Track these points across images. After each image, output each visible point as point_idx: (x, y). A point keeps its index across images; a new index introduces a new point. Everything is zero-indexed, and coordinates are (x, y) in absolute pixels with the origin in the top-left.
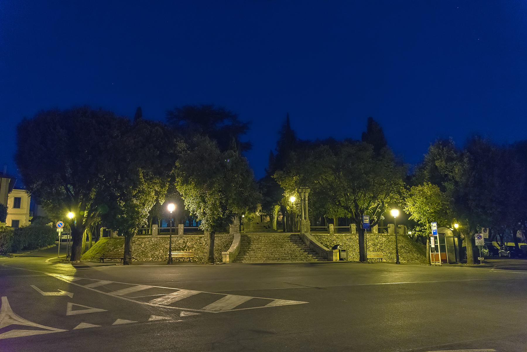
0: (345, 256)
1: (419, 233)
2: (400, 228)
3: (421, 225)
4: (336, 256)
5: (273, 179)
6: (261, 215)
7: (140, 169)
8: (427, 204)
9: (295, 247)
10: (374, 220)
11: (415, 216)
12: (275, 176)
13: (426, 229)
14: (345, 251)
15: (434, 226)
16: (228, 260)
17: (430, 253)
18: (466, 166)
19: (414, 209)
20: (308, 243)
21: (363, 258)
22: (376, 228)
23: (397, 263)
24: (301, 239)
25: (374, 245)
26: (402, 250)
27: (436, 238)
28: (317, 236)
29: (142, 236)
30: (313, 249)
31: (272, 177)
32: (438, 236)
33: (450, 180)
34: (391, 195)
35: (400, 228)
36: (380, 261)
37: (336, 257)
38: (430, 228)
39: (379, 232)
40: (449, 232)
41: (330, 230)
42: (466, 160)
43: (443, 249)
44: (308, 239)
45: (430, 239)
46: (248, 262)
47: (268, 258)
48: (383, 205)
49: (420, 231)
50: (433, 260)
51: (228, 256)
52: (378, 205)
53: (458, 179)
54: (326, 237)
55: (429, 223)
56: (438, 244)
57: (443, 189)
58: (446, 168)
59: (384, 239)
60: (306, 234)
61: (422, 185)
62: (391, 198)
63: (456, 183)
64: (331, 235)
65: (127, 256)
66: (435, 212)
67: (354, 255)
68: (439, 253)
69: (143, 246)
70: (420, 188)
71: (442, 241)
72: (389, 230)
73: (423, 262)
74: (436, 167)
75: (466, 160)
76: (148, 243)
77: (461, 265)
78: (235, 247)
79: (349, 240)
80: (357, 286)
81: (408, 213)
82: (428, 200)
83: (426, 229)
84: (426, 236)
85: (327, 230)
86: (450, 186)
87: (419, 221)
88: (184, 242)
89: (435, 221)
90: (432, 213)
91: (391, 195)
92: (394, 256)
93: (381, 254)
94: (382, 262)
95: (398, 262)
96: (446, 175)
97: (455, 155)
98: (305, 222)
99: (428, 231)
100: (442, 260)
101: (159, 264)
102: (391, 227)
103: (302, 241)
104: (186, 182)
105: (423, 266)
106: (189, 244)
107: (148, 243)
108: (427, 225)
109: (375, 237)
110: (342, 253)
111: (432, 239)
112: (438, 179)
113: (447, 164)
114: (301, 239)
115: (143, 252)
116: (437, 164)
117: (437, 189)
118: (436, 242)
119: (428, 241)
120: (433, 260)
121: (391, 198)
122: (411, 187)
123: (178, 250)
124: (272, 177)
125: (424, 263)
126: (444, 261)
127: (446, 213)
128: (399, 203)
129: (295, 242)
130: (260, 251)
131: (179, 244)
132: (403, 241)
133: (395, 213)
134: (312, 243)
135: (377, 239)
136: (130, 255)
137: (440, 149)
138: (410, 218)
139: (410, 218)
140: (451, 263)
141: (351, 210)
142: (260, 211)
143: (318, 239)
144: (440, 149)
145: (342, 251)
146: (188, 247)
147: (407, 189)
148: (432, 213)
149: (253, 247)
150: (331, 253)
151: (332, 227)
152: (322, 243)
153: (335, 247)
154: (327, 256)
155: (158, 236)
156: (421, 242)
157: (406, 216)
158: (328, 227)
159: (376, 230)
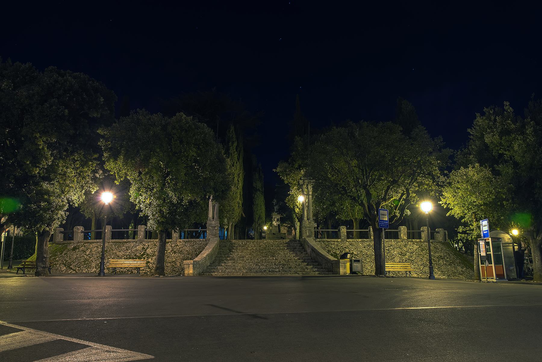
0: (359, 269)
1: (463, 235)
2: (438, 232)
3: (465, 225)
4: (345, 267)
5: (276, 173)
6: (279, 225)
7: (38, 135)
8: (472, 193)
9: (291, 256)
10: (396, 216)
11: (456, 211)
12: (278, 169)
13: (473, 230)
14: (359, 261)
15: (485, 225)
16: (191, 271)
17: (480, 265)
18: (531, 139)
19: (454, 202)
20: (309, 251)
21: (380, 269)
22: (403, 230)
23: (430, 278)
24: (301, 245)
25: (401, 254)
26: (441, 261)
27: (487, 244)
28: (324, 242)
29: (90, 241)
30: (316, 259)
31: (274, 170)
32: (490, 240)
33: (506, 161)
34: (420, 179)
35: (438, 232)
36: (407, 275)
37: (345, 269)
38: (479, 227)
39: (409, 237)
40: (506, 237)
41: (342, 234)
42: (529, 130)
43: (498, 260)
44: (309, 246)
45: (478, 245)
46: (220, 274)
47: (250, 270)
48: (408, 194)
49: (464, 232)
50: (484, 275)
51: (191, 266)
52: (403, 194)
53: (518, 159)
54: (336, 243)
55: (477, 220)
56: (492, 253)
57: (496, 173)
58: (501, 144)
59: (416, 247)
60: (307, 239)
61: (466, 167)
62: (421, 184)
63: (516, 165)
64: (342, 241)
65: (40, 264)
66: (485, 204)
67: (369, 268)
68: (493, 265)
69: (87, 253)
70: (462, 170)
71: (497, 248)
72: (423, 235)
73: (471, 278)
74: (486, 145)
75: (529, 130)
76: (95, 249)
77: (525, 281)
78: (205, 255)
79: (363, 248)
80: (373, 310)
81: (445, 207)
82: (475, 186)
83: (473, 230)
84: (472, 240)
85: (336, 235)
86: (507, 170)
87: (462, 218)
88: (143, 248)
89: (485, 218)
90: (481, 205)
91: (420, 179)
92: (427, 269)
93: (410, 267)
94: (410, 277)
95: (431, 277)
96: (501, 155)
97: (513, 126)
98: (310, 224)
99: (475, 233)
100: (497, 276)
101: (84, 276)
102: (425, 232)
103: (303, 248)
104: (115, 156)
105: (470, 282)
106: (149, 251)
107: (95, 249)
108: (475, 224)
109: (404, 243)
110: (355, 264)
111: (482, 243)
112: (489, 159)
113: (501, 139)
114: (301, 245)
115: (86, 260)
116: (487, 140)
117: (487, 172)
118: (487, 250)
119: (475, 246)
120: (484, 275)
121: (421, 184)
122: (450, 172)
123: (133, 258)
124: (274, 170)
125: (472, 279)
126: (500, 276)
127: (502, 206)
128: (432, 190)
129: (293, 250)
130: (243, 260)
131: (137, 250)
132: (429, 236)
133: (426, 207)
134: (313, 250)
135: (405, 246)
136: (44, 262)
137: (490, 120)
138: (448, 215)
139: (448, 215)
140: (510, 280)
141: (362, 202)
142: (278, 220)
143: (324, 246)
144: (490, 120)
145: (355, 261)
146: (148, 255)
147: (445, 175)
148: (481, 205)
149: (235, 255)
150: (337, 263)
151: (344, 230)
152: (329, 251)
153: (344, 256)
154: (332, 268)
155: (111, 241)
156: (466, 255)
157: (442, 211)
158: (339, 230)
159: (404, 235)
